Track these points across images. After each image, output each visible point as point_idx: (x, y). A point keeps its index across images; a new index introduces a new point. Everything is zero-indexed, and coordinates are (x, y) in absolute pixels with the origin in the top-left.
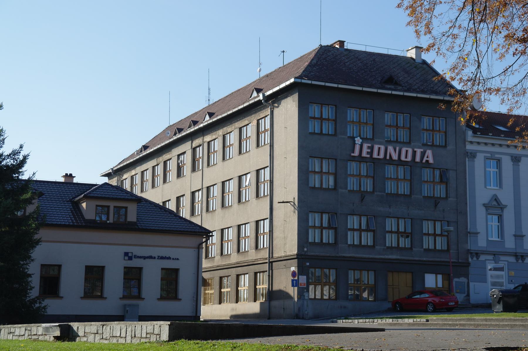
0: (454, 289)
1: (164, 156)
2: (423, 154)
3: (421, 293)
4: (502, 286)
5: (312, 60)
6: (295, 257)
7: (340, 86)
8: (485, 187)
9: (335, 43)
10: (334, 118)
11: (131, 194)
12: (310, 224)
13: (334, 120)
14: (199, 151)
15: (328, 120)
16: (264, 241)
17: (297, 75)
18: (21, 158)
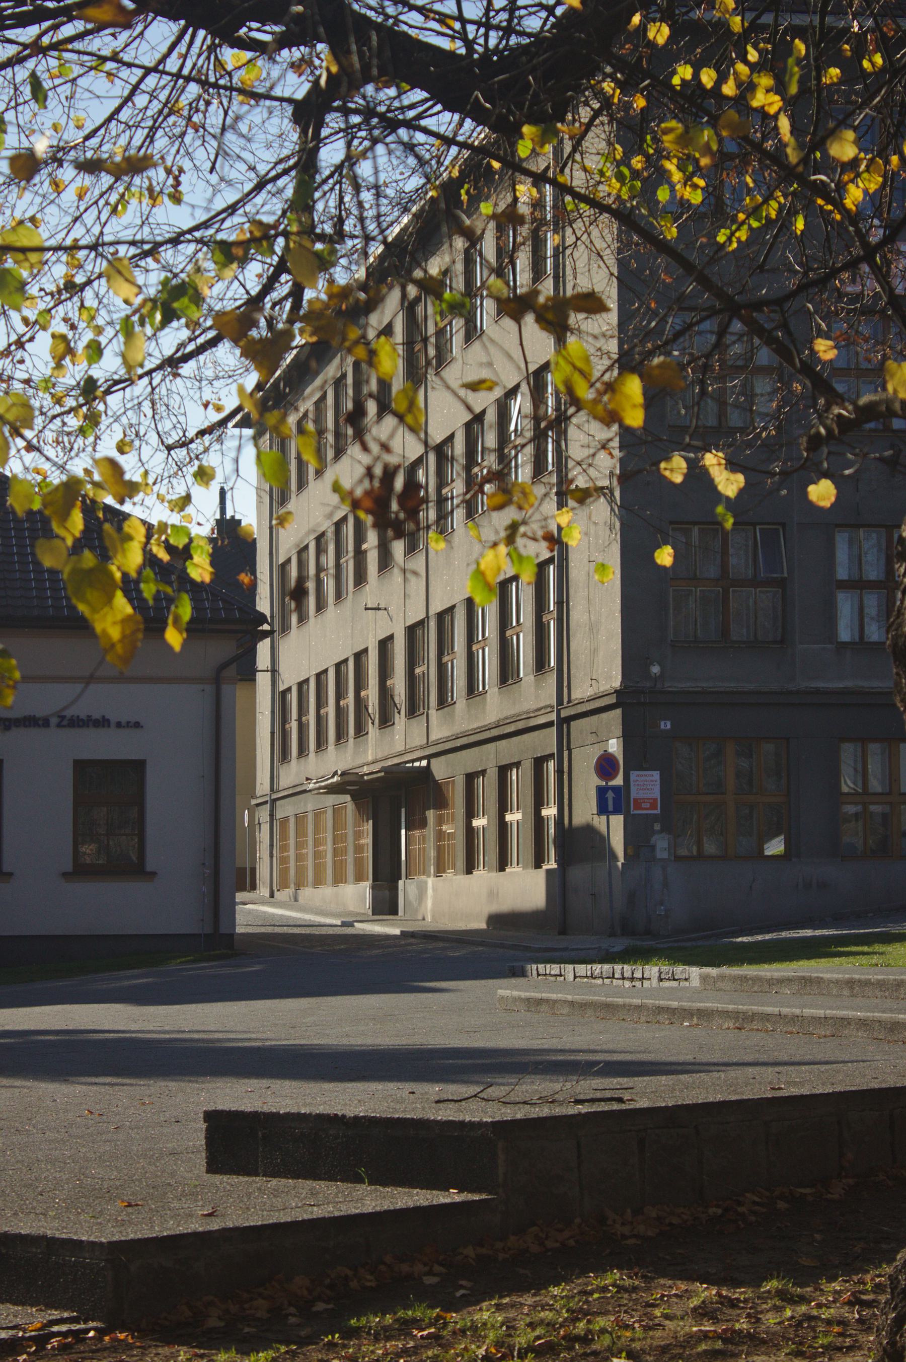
6: (612, 700)
12: (842, 573)
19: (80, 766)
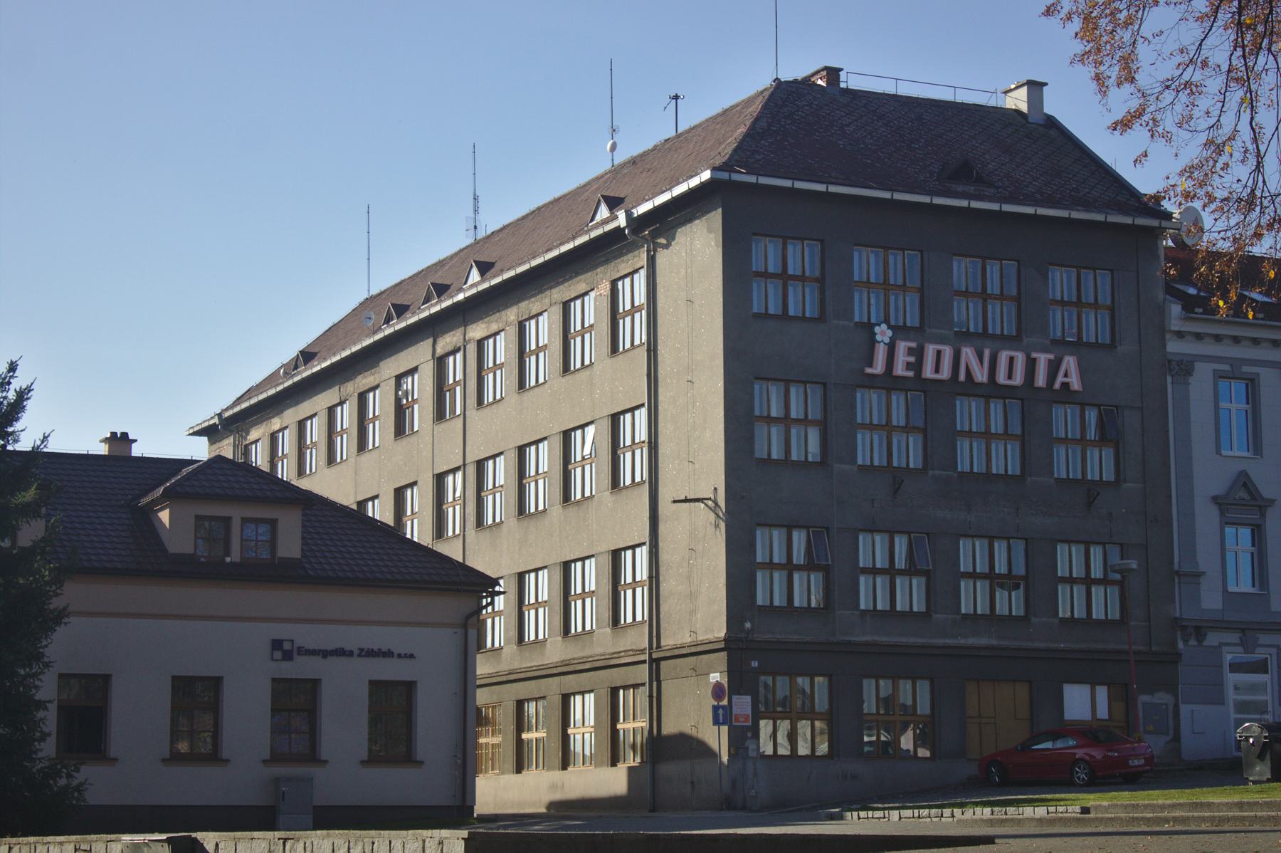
0: (1141, 722)
1: (360, 377)
2: (1054, 367)
3: (1055, 736)
4: (1262, 713)
5: (757, 119)
6: (722, 645)
7: (833, 189)
8: (1218, 452)
9: (813, 75)
10: (817, 274)
11: (270, 478)
13: (817, 280)
14: (455, 368)
15: (802, 278)
16: (635, 606)
17: (719, 161)
18: (11, 395)
19: (374, 684)
